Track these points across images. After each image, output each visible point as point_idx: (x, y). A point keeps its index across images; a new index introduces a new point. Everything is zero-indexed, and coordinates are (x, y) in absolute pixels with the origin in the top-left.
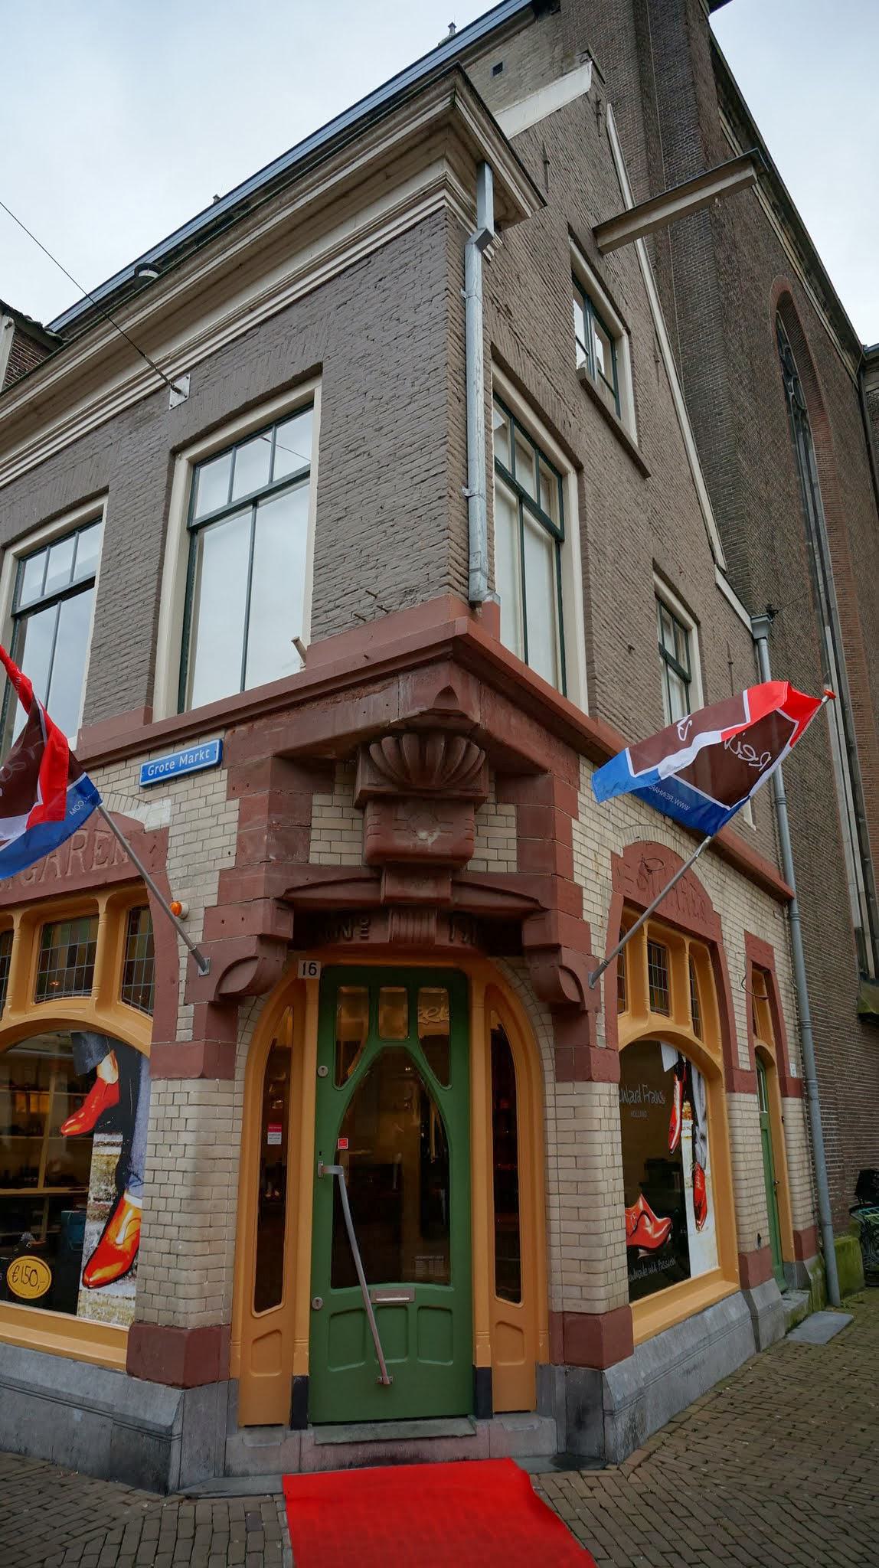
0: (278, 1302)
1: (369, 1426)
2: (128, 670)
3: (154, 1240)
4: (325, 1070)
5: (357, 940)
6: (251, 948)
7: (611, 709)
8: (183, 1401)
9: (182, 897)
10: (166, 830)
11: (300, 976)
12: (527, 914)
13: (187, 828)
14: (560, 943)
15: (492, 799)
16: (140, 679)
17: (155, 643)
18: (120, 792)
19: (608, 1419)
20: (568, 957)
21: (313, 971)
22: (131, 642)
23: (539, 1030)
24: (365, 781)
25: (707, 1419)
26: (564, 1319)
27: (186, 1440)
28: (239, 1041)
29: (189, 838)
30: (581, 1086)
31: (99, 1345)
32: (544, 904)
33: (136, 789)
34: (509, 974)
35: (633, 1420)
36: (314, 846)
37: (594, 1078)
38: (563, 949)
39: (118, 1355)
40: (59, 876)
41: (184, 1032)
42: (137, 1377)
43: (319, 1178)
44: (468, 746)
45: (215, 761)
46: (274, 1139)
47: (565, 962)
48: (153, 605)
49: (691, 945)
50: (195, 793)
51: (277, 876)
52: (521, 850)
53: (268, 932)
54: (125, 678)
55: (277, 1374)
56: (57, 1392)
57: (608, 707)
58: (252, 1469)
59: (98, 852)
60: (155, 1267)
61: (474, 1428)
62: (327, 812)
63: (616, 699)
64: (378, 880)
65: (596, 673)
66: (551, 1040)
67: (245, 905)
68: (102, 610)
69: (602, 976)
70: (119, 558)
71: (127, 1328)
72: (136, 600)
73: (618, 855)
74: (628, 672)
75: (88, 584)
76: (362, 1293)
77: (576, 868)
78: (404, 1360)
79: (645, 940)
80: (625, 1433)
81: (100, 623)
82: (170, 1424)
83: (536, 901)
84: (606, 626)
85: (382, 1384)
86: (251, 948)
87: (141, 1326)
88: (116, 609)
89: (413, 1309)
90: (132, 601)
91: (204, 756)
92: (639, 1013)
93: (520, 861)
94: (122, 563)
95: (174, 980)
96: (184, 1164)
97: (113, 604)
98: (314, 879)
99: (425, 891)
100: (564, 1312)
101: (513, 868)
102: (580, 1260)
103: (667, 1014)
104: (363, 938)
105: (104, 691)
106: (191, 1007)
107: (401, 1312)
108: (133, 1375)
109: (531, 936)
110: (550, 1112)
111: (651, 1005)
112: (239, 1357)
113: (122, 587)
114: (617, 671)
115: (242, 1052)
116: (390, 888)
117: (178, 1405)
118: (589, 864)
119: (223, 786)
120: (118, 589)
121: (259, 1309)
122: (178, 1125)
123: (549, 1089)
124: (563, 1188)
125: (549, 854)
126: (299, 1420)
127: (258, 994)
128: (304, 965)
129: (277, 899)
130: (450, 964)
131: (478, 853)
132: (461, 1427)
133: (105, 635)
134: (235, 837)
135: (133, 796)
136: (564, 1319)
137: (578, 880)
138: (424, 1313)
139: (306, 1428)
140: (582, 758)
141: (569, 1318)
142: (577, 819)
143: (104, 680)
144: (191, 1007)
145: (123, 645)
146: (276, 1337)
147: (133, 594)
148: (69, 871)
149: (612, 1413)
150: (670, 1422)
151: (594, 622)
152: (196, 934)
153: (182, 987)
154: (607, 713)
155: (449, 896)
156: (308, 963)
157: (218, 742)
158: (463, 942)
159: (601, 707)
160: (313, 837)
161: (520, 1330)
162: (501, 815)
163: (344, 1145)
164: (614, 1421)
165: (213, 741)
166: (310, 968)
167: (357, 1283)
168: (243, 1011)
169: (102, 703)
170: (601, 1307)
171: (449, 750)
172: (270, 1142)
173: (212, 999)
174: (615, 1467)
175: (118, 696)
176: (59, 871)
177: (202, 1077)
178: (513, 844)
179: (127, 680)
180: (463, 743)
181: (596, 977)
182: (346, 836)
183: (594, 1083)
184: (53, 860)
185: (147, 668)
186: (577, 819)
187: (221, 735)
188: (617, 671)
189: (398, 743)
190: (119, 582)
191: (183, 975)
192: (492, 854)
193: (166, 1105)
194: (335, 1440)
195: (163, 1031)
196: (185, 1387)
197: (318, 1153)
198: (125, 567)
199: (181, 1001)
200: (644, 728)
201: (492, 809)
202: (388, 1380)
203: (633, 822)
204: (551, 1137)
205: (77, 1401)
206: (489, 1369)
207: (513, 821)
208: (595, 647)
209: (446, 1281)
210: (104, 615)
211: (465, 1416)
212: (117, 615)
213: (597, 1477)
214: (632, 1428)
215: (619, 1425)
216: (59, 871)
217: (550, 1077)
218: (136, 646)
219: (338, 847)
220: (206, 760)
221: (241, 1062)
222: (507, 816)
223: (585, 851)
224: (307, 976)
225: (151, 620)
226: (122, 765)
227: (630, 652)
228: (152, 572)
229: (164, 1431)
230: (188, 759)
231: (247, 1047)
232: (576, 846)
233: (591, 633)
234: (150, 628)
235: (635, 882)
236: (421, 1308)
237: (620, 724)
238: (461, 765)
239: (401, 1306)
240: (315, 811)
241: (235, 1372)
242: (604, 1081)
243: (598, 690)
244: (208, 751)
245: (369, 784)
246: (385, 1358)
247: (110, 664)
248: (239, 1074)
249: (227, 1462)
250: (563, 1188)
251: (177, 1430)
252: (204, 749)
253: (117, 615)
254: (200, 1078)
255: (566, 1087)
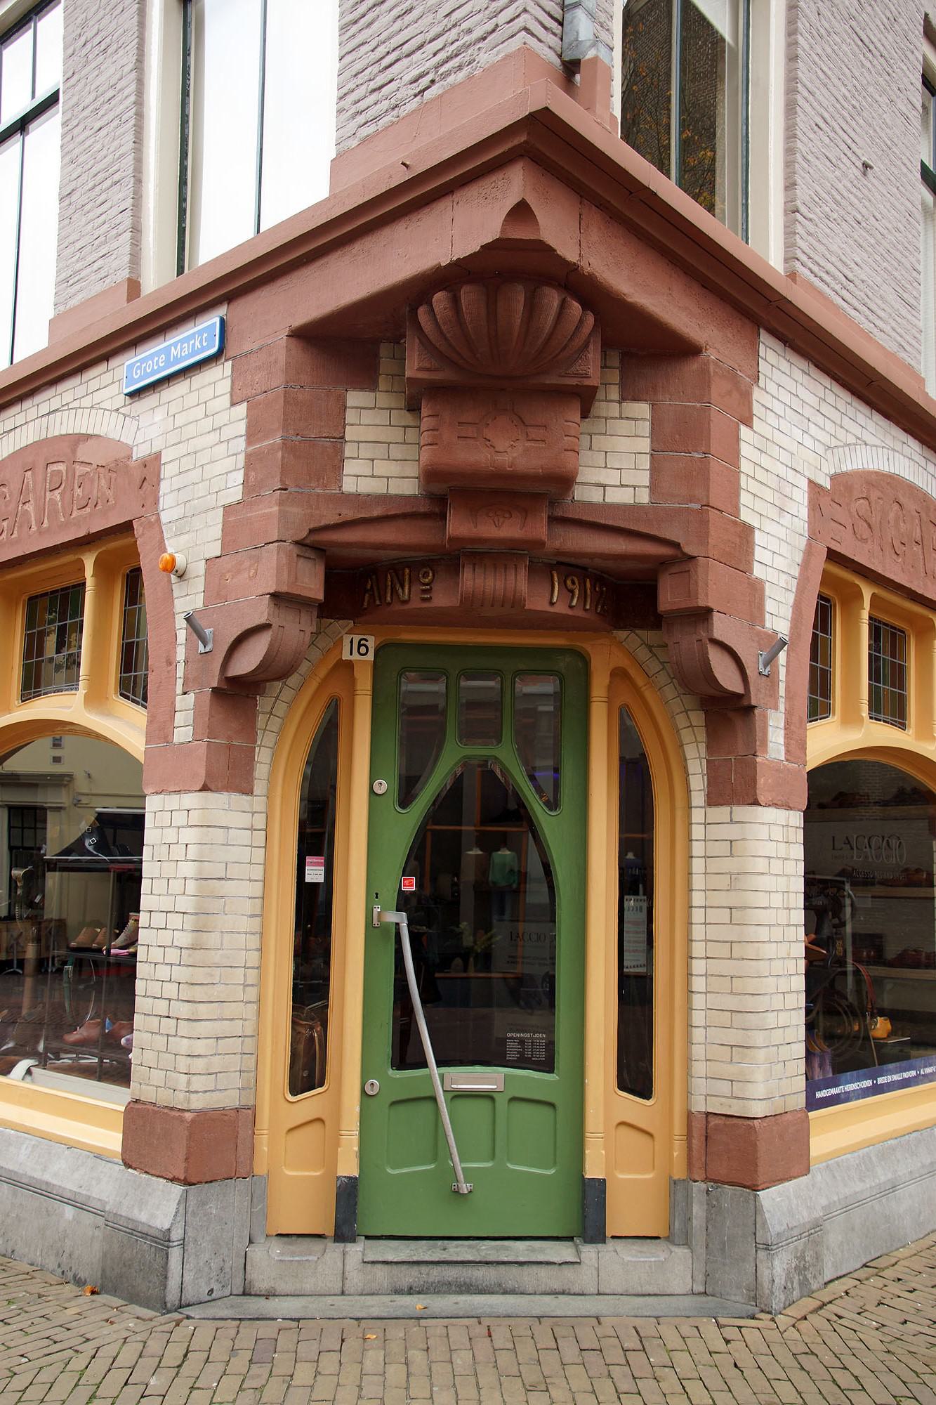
0: (321, 1085)
1: (440, 1243)
2: (106, 226)
3: (151, 1000)
4: (382, 787)
5: (415, 604)
6: (260, 612)
7: (823, 263)
8: (184, 1199)
9: (178, 548)
10: (158, 456)
11: (346, 656)
12: (663, 563)
13: (182, 449)
14: (710, 605)
15: (614, 393)
16: (121, 239)
17: (138, 181)
18: (102, 406)
19: (762, 1254)
20: (722, 627)
21: (363, 650)
22: (108, 183)
23: (686, 735)
24: (414, 366)
25: (917, 1268)
26: (707, 1122)
27: (190, 1247)
28: (259, 743)
29: (186, 463)
30: (742, 812)
31: (102, 1130)
32: (689, 550)
33: (121, 400)
34: (643, 654)
35: (802, 1258)
36: (350, 467)
37: (761, 799)
38: (716, 615)
39: (113, 1140)
40: (34, 528)
41: (183, 733)
42: (135, 1169)
43: (372, 928)
44: (563, 305)
45: (214, 350)
46: (315, 874)
47: (718, 634)
48: (132, 122)
49: (874, 597)
50: (192, 399)
51: (296, 511)
52: (655, 471)
53: (284, 589)
54: (102, 239)
55: (318, 1174)
56: (47, 1183)
57: (817, 258)
58: (281, 1287)
59: (78, 492)
60: (152, 1033)
61: (578, 1253)
62: (368, 417)
63: (834, 248)
64: (443, 517)
65: (798, 203)
66: (703, 747)
67: (253, 552)
68: (69, 137)
69: (782, 656)
70: (85, 51)
71: (122, 1109)
72: (111, 116)
73: (820, 486)
74: (860, 206)
75: (52, 100)
76: (430, 1077)
77: (744, 498)
78: (489, 1164)
79: (865, 615)
80: (788, 1275)
81: (68, 158)
82: (167, 1226)
83: (677, 546)
84: (822, 125)
85: (457, 1192)
86: (260, 612)
87: (137, 1106)
88: (87, 133)
89: (501, 1101)
90: (105, 118)
91: (201, 342)
92: (850, 719)
93: (654, 487)
94: (90, 57)
95: (170, 662)
96: (185, 904)
97: (81, 127)
98: (350, 514)
99: (507, 529)
100: (708, 1114)
101: (644, 497)
102: (732, 1046)
103: (903, 726)
104: (424, 600)
105: (78, 261)
106: (191, 697)
107: (485, 1105)
108: (130, 1167)
109: (669, 598)
110: (698, 848)
111: (870, 709)
112: (266, 1149)
113: (92, 97)
114: (838, 203)
115: (263, 756)
116: (458, 526)
117: (179, 1204)
118: (769, 495)
119: (226, 386)
120: (87, 102)
121: (294, 1092)
122: (178, 852)
123: (697, 815)
124: (714, 950)
125: (701, 474)
126: (344, 1231)
127: (283, 676)
128: (352, 642)
129: (297, 543)
130: (559, 641)
131: (585, 475)
132: (563, 1252)
133: (75, 175)
134: (242, 458)
135: (118, 410)
136: (707, 1122)
137: (746, 516)
138: (518, 1106)
139: (353, 1241)
140: (764, 337)
141: (714, 1122)
142: (751, 427)
143: (78, 245)
144: (191, 697)
145: (97, 189)
146: (317, 1126)
147: (106, 106)
148: (46, 521)
149: (767, 1247)
150: (865, 1266)
151: (800, 118)
152: (189, 599)
153: (180, 671)
154: (815, 269)
155: (545, 538)
156: (357, 638)
157: (217, 320)
158: (571, 607)
159: (803, 258)
160: (347, 454)
161: (650, 1135)
162: (627, 418)
163: (410, 885)
164: (770, 1258)
165: (211, 321)
166: (360, 645)
167: (423, 1064)
168: (263, 703)
169: (76, 279)
170: (758, 1110)
171: (532, 307)
172: (308, 879)
173: (215, 685)
174: (769, 1316)
175: (96, 266)
176: (33, 523)
177: (205, 788)
178: (645, 462)
179: (105, 242)
180: (552, 298)
181: (771, 660)
182: (396, 451)
183: (760, 808)
184: (26, 507)
185: (128, 222)
186: (751, 427)
187: (222, 311)
188: (838, 203)
189: (455, 301)
190: (87, 89)
191: (181, 654)
192: (611, 477)
193: (162, 828)
194: (390, 1258)
195: (159, 731)
196: (187, 1183)
197: (373, 895)
198: (93, 65)
199: (179, 690)
200: (882, 298)
201: (614, 409)
202: (465, 1188)
203: (851, 440)
204: (698, 882)
205: (68, 1195)
206: (603, 1182)
207: (645, 427)
208: (800, 159)
209: (547, 1065)
210: (71, 146)
211: (570, 1239)
212: (88, 143)
213: (739, 1327)
214: (801, 1269)
215: (776, 1262)
216: (33, 523)
217: (698, 798)
218: (116, 188)
219: (382, 468)
220: (203, 349)
221: (261, 770)
222: (636, 419)
223: (760, 475)
224: (356, 656)
225: (131, 145)
226: (102, 367)
227: (865, 174)
228: (127, 69)
229: (160, 1236)
230: (181, 349)
231: (269, 751)
232: (745, 466)
233: (795, 136)
234: (130, 160)
235: (850, 528)
236: (514, 1099)
237: (838, 287)
238: (551, 334)
239: (488, 1096)
240: (350, 416)
241: (260, 1168)
242: (776, 805)
243: (799, 229)
244: (205, 335)
245: (419, 370)
246: (461, 1161)
247: (84, 219)
248: (259, 787)
249: (248, 1276)
250: (714, 950)
251: (176, 1235)
252: (200, 333)
253: (88, 143)
254: (200, 790)
255: (721, 813)
